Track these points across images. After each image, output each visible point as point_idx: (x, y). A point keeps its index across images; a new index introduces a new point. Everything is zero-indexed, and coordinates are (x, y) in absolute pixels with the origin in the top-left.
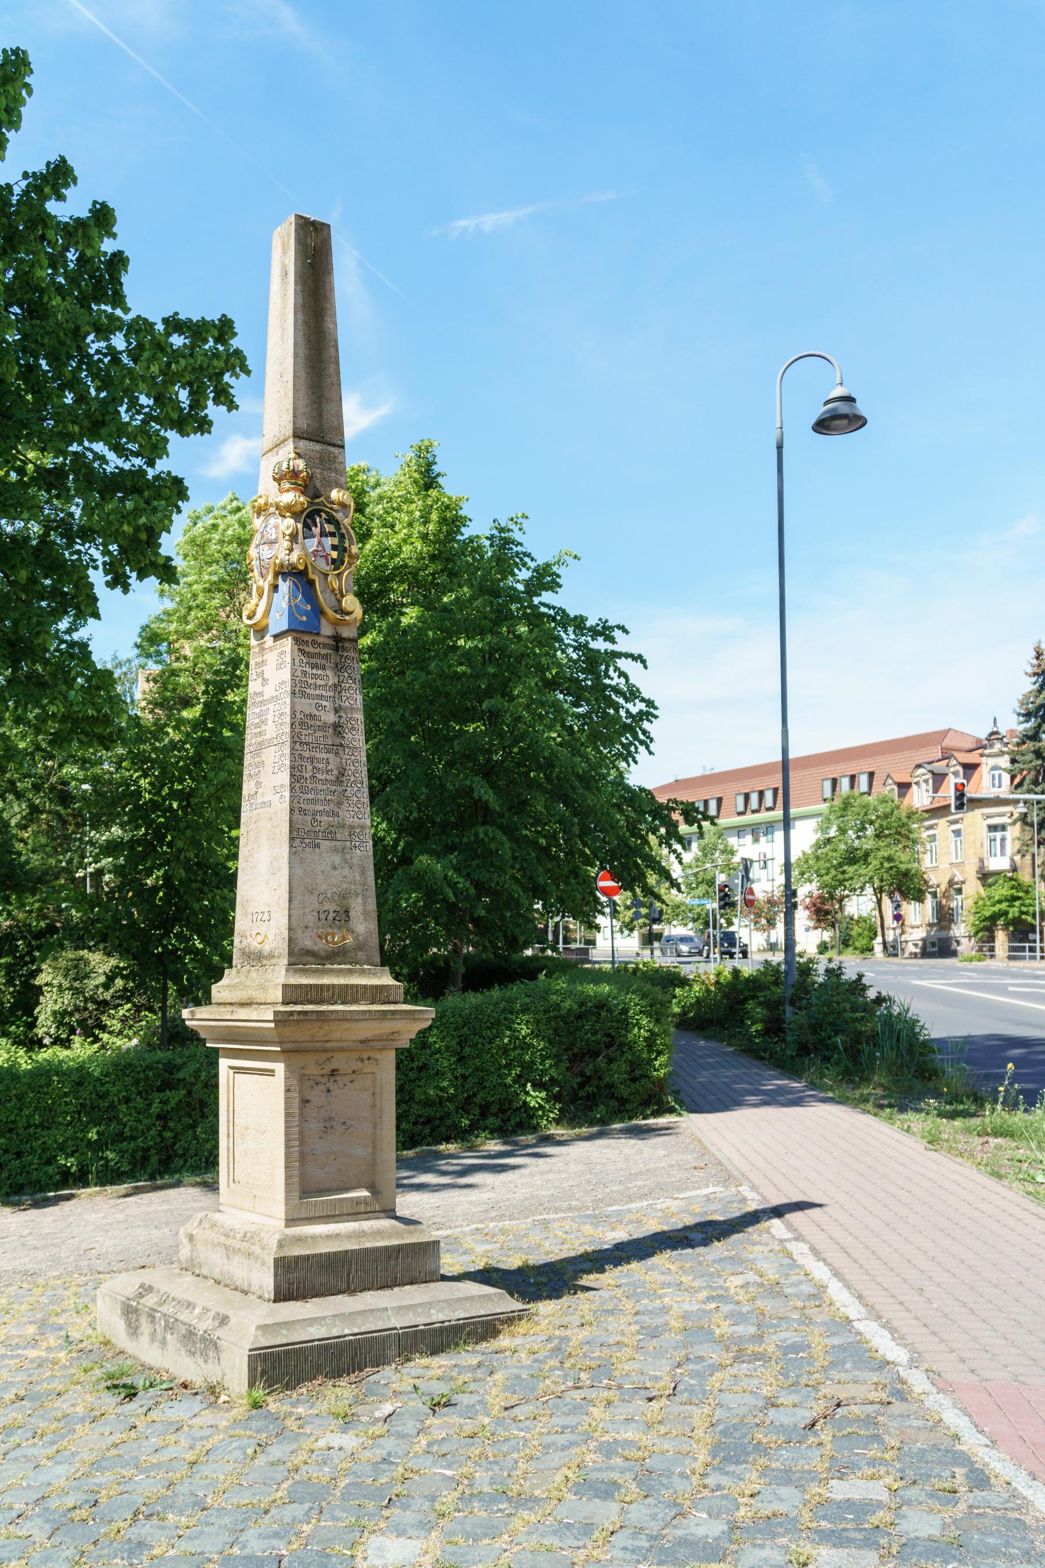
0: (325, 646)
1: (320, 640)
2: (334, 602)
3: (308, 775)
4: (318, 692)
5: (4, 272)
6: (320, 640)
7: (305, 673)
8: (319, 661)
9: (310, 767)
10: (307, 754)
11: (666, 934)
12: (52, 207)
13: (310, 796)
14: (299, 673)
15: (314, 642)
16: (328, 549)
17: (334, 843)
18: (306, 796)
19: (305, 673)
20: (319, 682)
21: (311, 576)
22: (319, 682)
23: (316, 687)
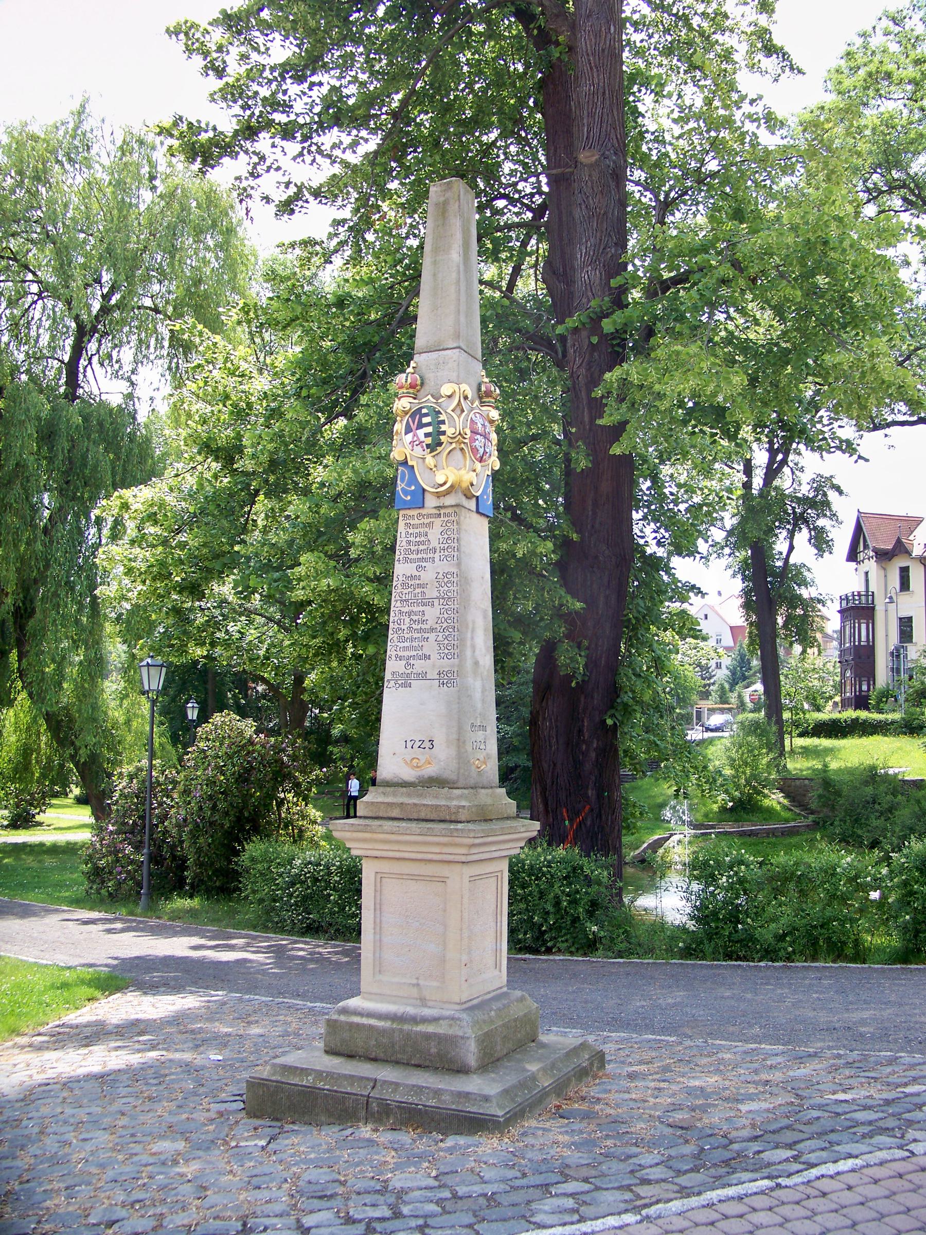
0: (429, 516)
1: (423, 511)
4: (420, 556)
7: (409, 542)
9: (407, 620)
10: (406, 609)
13: (406, 644)
16: (422, 438)
18: (402, 645)
19: (409, 542)
20: (421, 547)
22: (421, 547)
23: (418, 552)
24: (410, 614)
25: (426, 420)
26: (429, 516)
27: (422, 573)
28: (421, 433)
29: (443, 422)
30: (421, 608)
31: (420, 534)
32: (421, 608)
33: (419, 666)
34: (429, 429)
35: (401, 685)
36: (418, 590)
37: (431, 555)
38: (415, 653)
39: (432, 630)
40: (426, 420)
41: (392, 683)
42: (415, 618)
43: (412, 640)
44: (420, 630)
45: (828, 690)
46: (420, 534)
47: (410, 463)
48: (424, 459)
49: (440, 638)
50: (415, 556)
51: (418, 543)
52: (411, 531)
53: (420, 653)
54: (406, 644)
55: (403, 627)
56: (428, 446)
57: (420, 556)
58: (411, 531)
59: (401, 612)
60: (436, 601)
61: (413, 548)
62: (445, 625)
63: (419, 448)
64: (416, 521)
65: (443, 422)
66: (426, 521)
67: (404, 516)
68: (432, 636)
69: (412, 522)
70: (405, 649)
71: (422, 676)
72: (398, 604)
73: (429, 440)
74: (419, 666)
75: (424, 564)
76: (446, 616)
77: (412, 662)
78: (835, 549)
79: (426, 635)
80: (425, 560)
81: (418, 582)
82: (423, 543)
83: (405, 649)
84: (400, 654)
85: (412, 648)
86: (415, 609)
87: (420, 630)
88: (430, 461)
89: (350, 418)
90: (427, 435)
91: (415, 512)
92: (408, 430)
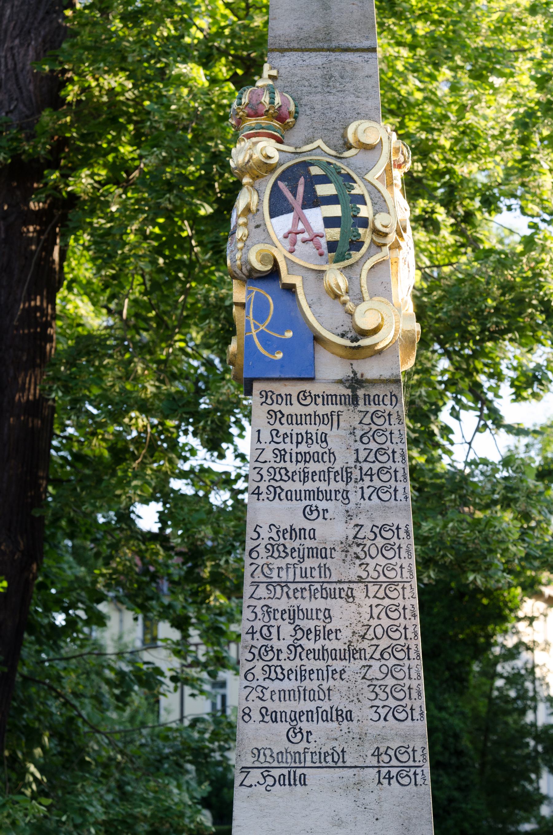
0: (327, 399)
1: (315, 389)
2: (340, 317)
3: (282, 645)
4: (310, 485)
5: (90, 832)
6: (315, 389)
7: (281, 455)
8: (312, 429)
9: (287, 629)
10: (283, 604)
11: (527, 95)
12: (172, 480)
13: (287, 685)
14: (268, 455)
15: (303, 396)
16: (318, 226)
17: (339, 772)
18: (276, 685)
19: (281, 455)
20: (313, 467)
21: (286, 278)
22: (313, 467)
23: (305, 477)
24: (293, 615)
25: (324, 190)
26: (327, 399)
27: (319, 525)
28: (315, 217)
29: (361, 199)
30: (321, 604)
31: (308, 438)
32: (321, 604)
33: (322, 733)
34: (335, 211)
35: (280, 781)
36: (309, 563)
37: (341, 486)
38: (311, 706)
39: (352, 653)
40: (324, 190)
41: (255, 776)
42: (306, 624)
43: (303, 674)
44: (322, 654)
45: (519, 525)
46: (308, 438)
47: (286, 278)
48: (321, 273)
49: (374, 673)
50: (297, 486)
51: (305, 457)
52: (284, 429)
53: (326, 705)
54: (287, 685)
55: (276, 644)
56: (332, 246)
57: (310, 485)
58: (284, 429)
59: (268, 611)
60: (359, 590)
61: (292, 467)
62: (384, 643)
63: (310, 248)
64: (296, 409)
65: (361, 199)
66: (323, 410)
67: (265, 395)
68: (354, 666)
69: (287, 410)
70: (284, 695)
71: (334, 760)
72: (262, 591)
73: (334, 233)
74: (322, 733)
75: (323, 505)
76: (385, 622)
77: (305, 726)
78: (516, 404)
79: (338, 665)
80: (327, 496)
81: (309, 543)
82: (317, 458)
83: (284, 695)
84: (272, 706)
85: (304, 694)
86: (305, 604)
87: (322, 654)
88: (336, 278)
89: (249, 55)
90: (330, 222)
91: (293, 389)
92: (278, 207)
